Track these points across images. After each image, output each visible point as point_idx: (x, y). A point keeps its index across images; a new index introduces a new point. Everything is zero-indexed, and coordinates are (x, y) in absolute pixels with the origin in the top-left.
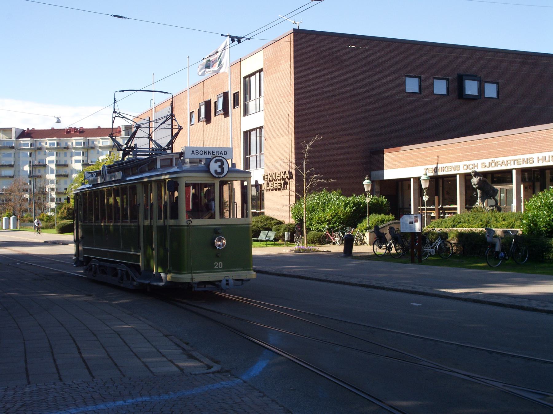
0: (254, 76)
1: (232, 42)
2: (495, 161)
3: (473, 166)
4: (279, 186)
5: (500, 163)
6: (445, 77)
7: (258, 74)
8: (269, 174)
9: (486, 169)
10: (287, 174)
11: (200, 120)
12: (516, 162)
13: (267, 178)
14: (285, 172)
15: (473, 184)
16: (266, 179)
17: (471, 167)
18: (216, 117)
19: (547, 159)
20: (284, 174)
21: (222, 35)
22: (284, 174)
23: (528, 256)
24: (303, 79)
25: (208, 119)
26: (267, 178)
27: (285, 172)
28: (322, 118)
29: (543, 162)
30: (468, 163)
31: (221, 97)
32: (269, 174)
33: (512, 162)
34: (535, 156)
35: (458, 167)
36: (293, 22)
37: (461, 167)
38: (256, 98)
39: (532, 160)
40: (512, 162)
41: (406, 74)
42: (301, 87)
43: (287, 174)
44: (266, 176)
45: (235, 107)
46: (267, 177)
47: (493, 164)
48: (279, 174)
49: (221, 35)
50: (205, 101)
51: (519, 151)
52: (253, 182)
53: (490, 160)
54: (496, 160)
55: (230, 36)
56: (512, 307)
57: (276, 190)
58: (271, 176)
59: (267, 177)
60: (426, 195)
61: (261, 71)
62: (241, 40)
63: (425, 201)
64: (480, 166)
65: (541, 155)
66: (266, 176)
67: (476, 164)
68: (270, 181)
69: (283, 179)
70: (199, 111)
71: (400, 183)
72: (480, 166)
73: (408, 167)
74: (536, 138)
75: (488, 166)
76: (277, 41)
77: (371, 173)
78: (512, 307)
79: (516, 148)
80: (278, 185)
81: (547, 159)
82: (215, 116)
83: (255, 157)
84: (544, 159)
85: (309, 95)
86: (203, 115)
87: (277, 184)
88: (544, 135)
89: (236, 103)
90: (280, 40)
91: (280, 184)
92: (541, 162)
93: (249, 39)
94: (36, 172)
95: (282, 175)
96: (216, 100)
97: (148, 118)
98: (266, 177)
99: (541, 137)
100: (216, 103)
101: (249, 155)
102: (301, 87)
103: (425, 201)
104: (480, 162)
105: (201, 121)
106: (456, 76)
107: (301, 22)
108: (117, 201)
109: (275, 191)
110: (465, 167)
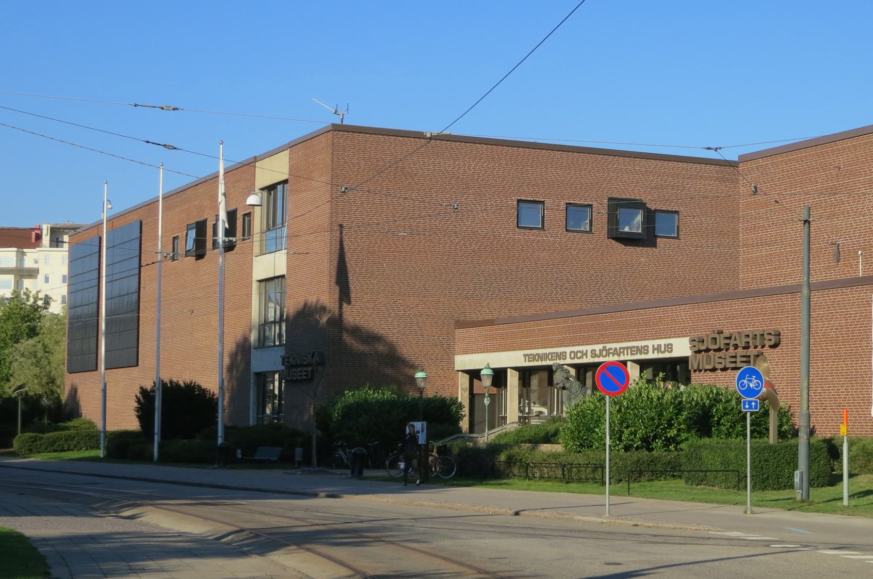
3: (581, 355)
5: (612, 351)
12: (629, 350)
13: (288, 362)
17: (579, 355)
20: (313, 357)
22: (313, 357)
23: (455, 470)
24: (347, 205)
26: (288, 362)
27: (313, 354)
28: (376, 267)
30: (576, 349)
31: (193, 228)
34: (650, 343)
35: (562, 356)
36: (334, 111)
37: (650, 349)
41: (519, 198)
42: (342, 218)
44: (287, 358)
46: (287, 360)
47: (604, 353)
53: (600, 346)
54: (609, 346)
56: (22, 468)
58: (293, 359)
59: (287, 360)
61: (285, 182)
63: (487, 405)
65: (656, 342)
66: (287, 358)
67: (585, 352)
76: (246, 165)
78: (22, 468)
84: (658, 349)
85: (355, 231)
86: (190, 245)
91: (305, 373)
97: (98, 238)
102: (342, 218)
106: (606, 201)
107: (347, 112)
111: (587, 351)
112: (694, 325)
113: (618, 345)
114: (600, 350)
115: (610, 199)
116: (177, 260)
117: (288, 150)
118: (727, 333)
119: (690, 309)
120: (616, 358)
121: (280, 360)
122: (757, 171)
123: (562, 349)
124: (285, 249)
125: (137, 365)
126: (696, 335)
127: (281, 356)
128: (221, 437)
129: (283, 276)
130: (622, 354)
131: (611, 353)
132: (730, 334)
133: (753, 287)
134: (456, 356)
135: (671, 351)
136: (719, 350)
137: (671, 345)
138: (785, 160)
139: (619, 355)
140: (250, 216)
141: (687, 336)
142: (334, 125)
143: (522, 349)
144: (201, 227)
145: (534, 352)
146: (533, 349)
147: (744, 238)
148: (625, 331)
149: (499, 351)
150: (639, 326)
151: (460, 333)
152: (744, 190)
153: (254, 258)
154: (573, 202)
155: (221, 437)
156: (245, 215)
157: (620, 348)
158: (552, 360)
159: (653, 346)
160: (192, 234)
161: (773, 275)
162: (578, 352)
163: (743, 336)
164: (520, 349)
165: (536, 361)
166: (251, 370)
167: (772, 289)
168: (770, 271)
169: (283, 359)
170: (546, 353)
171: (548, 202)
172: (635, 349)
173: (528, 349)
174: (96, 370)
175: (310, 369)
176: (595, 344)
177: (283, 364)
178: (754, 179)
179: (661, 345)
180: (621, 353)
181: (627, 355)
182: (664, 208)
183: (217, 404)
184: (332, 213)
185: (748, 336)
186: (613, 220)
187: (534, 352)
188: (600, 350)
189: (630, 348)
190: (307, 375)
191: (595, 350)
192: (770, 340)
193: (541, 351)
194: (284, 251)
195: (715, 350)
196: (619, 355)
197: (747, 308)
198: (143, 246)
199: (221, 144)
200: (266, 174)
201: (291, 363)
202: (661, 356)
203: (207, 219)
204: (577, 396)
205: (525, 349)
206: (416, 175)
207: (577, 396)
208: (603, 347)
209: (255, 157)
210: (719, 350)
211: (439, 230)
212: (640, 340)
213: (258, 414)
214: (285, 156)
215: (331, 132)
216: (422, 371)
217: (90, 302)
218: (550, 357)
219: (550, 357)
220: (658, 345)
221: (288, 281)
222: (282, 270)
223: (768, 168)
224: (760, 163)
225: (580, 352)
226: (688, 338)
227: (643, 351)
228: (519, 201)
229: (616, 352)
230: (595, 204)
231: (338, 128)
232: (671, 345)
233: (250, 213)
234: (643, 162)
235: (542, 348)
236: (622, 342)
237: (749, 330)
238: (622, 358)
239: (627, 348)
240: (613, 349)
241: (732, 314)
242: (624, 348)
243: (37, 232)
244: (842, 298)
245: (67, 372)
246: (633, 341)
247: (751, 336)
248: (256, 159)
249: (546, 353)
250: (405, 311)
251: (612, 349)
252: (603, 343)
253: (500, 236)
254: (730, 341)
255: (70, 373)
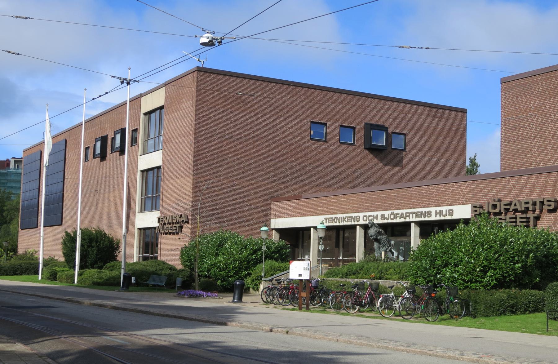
0: (154, 113)
1: (122, 84)
2: (395, 213)
4: (174, 229)
5: (400, 215)
6: (351, 126)
7: (158, 112)
8: (165, 217)
9: (385, 221)
10: (183, 218)
11: (96, 157)
12: (414, 215)
13: (162, 221)
14: (181, 215)
15: (370, 235)
16: (161, 222)
17: (370, 218)
18: (113, 154)
19: (444, 213)
20: (180, 217)
21: (112, 77)
25: (103, 157)
26: (162, 221)
29: (440, 216)
30: (368, 214)
32: (165, 217)
33: (411, 215)
34: (433, 210)
35: (358, 218)
36: (198, 60)
38: (155, 135)
39: (429, 214)
40: (411, 215)
41: (312, 120)
43: (183, 218)
44: (162, 218)
45: (134, 145)
46: (162, 220)
48: (175, 217)
49: (110, 76)
50: (101, 137)
51: (418, 204)
52: (159, 224)
53: (389, 212)
54: (396, 212)
55: (120, 78)
57: (170, 234)
58: (166, 219)
59: (162, 220)
60: (322, 244)
61: (161, 108)
62: (130, 82)
63: (321, 250)
64: (379, 217)
65: (438, 209)
66: (162, 218)
68: (165, 224)
69: (178, 223)
70: (95, 146)
71: (301, 232)
72: (379, 217)
73: (309, 216)
74: (434, 191)
75: (387, 217)
77: (271, 221)
79: (415, 201)
80: (174, 228)
81: (444, 213)
82: (112, 153)
83: (151, 198)
84: (440, 213)
86: (98, 151)
87: (172, 227)
88: (443, 189)
89: (134, 141)
90: (170, 84)
91: (175, 228)
92: (438, 216)
93: (138, 81)
94: (137, 334)
95: (178, 218)
96: (113, 136)
98: (161, 220)
99: (440, 191)
100: (113, 139)
101: (156, 193)
103: (321, 250)
104: (379, 213)
105: (97, 158)
106: (363, 125)
108: (507, 289)
109: (169, 234)
110: (365, 218)
111: (377, 215)
112: (473, 196)
113: (404, 211)
114: (389, 214)
115: (366, 124)
116: (88, 161)
117: (165, 87)
118: (505, 200)
119: (469, 184)
120: (402, 220)
121: (157, 219)
122: (518, 88)
123: (375, 213)
124: (161, 150)
125: (61, 224)
126: (478, 203)
127: (157, 218)
128: (124, 269)
129: (159, 168)
130: (408, 218)
131: (399, 217)
132: (510, 202)
133: (546, 165)
134: (271, 219)
135: (452, 215)
136: (500, 213)
137: (452, 210)
138: (545, 78)
139: (405, 218)
140: (137, 132)
141: (470, 204)
142: (198, 67)
143: (324, 215)
144: (104, 140)
145: (333, 216)
146: (332, 214)
147: (505, 136)
148: (410, 202)
149: (305, 216)
150: (423, 197)
151: (274, 205)
152: (506, 102)
153: (139, 157)
154: (344, 125)
155: (124, 269)
156: (133, 131)
157: (406, 213)
158: (348, 222)
159: (436, 211)
160: (99, 144)
161: (532, 161)
162: (369, 216)
163: (523, 203)
164: (321, 215)
165: (335, 222)
166: (136, 227)
167: (539, 169)
168: (530, 158)
169: (159, 219)
170: (343, 217)
171: (329, 124)
172: (420, 214)
173: (329, 214)
174: (37, 227)
175: (178, 225)
176: (385, 210)
177: (159, 222)
178: (515, 93)
179: (442, 211)
180: (406, 216)
181: (413, 218)
182: (397, 131)
183: (118, 247)
184: (196, 124)
185: (527, 203)
186: (368, 138)
187: (333, 216)
188: (389, 214)
189: (415, 213)
190: (176, 229)
191: (384, 215)
192: (550, 205)
193: (339, 216)
194: (161, 151)
195: (495, 214)
196: (405, 218)
197: (524, 182)
198: (67, 154)
199: (129, 69)
200: (148, 104)
201: (165, 222)
202: (442, 218)
203: (108, 135)
204: (385, 245)
205: (326, 215)
206: (249, 102)
207: (385, 245)
208: (392, 212)
209: (141, 94)
210: (500, 213)
211: (262, 138)
212: (424, 207)
213: (139, 254)
214: (162, 91)
215: (196, 72)
216: (266, 226)
217: (34, 198)
218: (346, 219)
219: (346, 219)
220: (440, 211)
221: (162, 170)
222: (159, 163)
223: (528, 85)
224: (521, 82)
225: (371, 216)
226: (470, 205)
227: (426, 215)
228: (312, 122)
229: (402, 216)
230: (357, 127)
231: (200, 70)
232: (452, 210)
233: (137, 129)
234: (386, 102)
235: (339, 214)
236: (407, 209)
237: (528, 198)
238: (408, 220)
239: (412, 213)
240: (400, 214)
241: (509, 187)
242: (409, 213)
243: (8, 162)
244: (440, 199)
245: (20, 228)
246: (418, 208)
247: (531, 203)
248: (141, 96)
249: (343, 217)
250: (240, 190)
251: (399, 214)
252: (391, 210)
253: (300, 144)
254: (510, 207)
255: (22, 229)
